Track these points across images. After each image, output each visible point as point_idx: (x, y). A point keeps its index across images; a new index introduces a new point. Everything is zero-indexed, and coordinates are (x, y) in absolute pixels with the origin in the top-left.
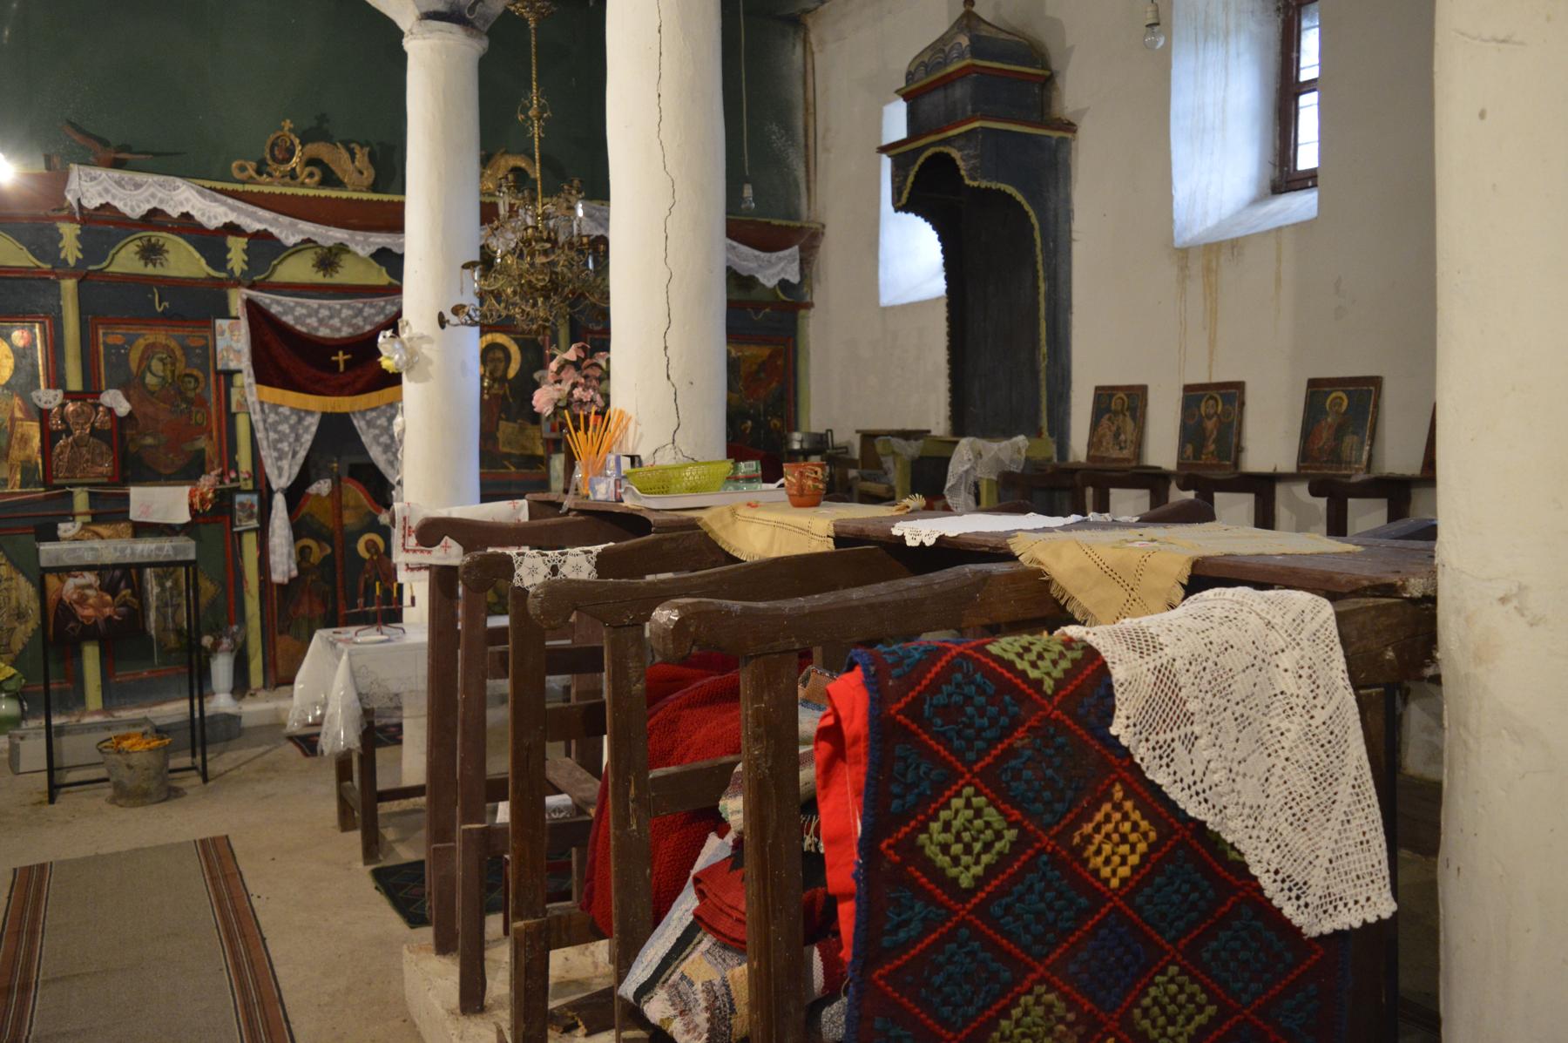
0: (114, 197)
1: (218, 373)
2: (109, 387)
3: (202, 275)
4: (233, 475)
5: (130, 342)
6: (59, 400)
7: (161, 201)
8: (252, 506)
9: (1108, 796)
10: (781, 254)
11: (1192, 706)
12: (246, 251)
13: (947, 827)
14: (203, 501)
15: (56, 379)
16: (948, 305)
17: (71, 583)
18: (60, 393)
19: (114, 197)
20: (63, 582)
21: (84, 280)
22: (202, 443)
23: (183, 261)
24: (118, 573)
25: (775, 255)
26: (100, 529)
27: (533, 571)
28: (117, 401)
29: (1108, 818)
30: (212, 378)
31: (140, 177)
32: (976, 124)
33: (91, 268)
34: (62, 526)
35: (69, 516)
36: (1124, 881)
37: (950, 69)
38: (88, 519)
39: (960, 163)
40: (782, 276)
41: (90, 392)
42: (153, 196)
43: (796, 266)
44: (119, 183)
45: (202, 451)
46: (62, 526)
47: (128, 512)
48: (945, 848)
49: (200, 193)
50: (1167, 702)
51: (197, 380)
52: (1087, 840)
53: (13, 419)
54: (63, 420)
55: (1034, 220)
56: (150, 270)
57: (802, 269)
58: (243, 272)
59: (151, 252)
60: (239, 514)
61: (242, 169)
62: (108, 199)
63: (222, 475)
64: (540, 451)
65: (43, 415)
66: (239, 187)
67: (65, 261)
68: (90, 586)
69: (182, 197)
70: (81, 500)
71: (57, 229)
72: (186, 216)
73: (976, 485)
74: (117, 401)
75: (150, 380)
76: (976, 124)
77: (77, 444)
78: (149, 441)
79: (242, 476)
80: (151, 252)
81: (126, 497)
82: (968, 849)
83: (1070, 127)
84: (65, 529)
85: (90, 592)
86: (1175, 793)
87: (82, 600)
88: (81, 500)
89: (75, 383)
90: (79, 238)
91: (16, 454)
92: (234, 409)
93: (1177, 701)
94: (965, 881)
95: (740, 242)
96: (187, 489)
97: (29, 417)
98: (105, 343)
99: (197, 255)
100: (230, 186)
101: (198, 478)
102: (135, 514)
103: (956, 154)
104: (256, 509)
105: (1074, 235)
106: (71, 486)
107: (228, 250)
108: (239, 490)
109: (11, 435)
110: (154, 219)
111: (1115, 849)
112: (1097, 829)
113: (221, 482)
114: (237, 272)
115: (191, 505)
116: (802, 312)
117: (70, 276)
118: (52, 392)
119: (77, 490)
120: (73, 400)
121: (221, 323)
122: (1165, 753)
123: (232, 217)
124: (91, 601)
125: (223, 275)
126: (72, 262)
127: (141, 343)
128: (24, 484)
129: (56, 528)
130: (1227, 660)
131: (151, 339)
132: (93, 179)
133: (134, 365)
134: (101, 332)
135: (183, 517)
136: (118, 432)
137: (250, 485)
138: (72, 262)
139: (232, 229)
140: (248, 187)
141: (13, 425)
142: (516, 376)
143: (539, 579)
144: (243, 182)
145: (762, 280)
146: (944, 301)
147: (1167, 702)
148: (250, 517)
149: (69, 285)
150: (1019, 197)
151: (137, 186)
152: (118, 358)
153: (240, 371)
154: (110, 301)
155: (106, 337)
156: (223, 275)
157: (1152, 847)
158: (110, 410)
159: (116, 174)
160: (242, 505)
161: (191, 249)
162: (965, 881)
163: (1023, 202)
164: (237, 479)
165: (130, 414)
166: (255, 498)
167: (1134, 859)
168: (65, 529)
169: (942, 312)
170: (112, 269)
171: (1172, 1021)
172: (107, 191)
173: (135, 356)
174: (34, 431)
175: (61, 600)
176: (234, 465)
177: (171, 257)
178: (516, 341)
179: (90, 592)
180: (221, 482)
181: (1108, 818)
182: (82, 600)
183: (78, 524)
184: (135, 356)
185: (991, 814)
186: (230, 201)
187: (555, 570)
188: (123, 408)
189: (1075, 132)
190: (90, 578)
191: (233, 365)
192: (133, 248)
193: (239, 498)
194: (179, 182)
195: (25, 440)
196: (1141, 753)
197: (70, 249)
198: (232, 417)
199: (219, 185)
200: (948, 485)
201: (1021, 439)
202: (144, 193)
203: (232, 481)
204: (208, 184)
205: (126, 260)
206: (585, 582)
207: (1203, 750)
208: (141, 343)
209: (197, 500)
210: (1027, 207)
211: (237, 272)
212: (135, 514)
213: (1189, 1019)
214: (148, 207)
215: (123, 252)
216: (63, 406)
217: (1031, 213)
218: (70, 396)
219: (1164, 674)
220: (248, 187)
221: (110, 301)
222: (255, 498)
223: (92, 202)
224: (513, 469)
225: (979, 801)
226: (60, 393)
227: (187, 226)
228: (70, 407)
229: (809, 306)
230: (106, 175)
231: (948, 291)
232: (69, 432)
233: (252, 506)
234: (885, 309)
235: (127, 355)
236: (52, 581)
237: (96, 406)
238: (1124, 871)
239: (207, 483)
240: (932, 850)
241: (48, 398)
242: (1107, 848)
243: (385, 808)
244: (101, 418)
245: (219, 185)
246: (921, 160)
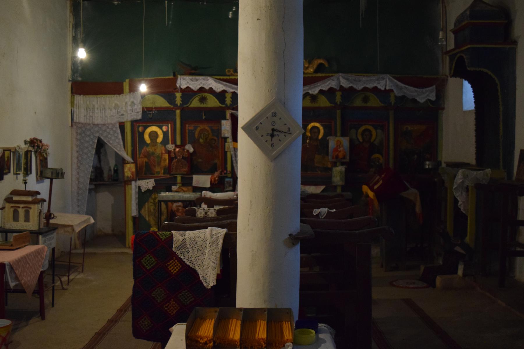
0: (190, 84)
1: (222, 138)
2: (189, 143)
3: (218, 106)
4: (225, 172)
5: (196, 128)
6: (174, 148)
7: (203, 84)
8: (230, 182)
9: (173, 259)
10: (427, 89)
11: (188, 246)
12: (231, 98)
13: (146, 260)
14: (215, 180)
15: (174, 142)
16: (475, 113)
17: (175, 205)
18: (174, 145)
19: (190, 84)
20: (173, 204)
21: (182, 110)
22: (216, 161)
23: (212, 102)
24: (188, 203)
25: (425, 90)
26: (184, 188)
27: (201, 213)
28: (190, 148)
29: (172, 262)
30: (220, 140)
31: (198, 77)
32: (469, 46)
33: (185, 106)
34: (173, 187)
35: (175, 184)
36: (175, 273)
37: (463, 24)
38: (181, 185)
39: (466, 60)
40: (428, 98)
41: (183, 144)
42: (201, 83)
43: (434, 94)
44: (192, 80)
45: (216, 164)
46: (173, 187)
47: (192, 183)
48: (145, 263)
49: (215, 81)
50: (183, 245)
51: (215, 140)
52: (169, 265)
53: (162, 153)
54: (175, 154)
55: (497, 82)
56: (202, 105)
57: (437, 96)
58: (230, 104)
59: (203, 100)
60: (227, 185)
61: (229, 71)
62: (188, 85)
63: (222, 171)
64: (330, 166)
65: (169, 152)
66: (228, 77)
67: (177, 104)
68: (180, 206)
69: (210, 83)
70: (179, 179)
71: (175, 95)
72: (211, 89)
73: (467, 188)
74: (190, 148)
75: (201, 140)
76: (469, 46)
77: (178, 161)
78: (200, 160)
79: (228, 172)
80: (203, 100)
81: (192, 178)
82: (149, 263)
83: (515, 43)
84: (174, 188)
85: (180, 208)
86: (184, 260)
87: (178, 210)
88: (179, 179)
89: (178, 143)
90: (181, 97)
91: (163, 164)
92: (226, 150)
93: (186, 245)
94: (148, 268)
95: (409, 85)
96: (210, 176)
97: (166, 153)
98: (188, 130)
99: (216, 100)
100: (225, 77)
101: (214, 173)
102: (194, 184)
103: (465, 57)
104: (232, 183)
105: (517, 87)
106: (177, 174)
107: (226, 98)
108: (227, 177)
109: (161, 158)
110: (202, 90)
111: (174, 268)
112: (171, 264)
113: (221, 174)
114: (228, 104)
115: (211, 182)
116: (440, 111)
117: (178, 109)
118: (172, 145)
119: (178, 176)
120: (178, 148)
121: (223, 122)
122: (183, 253)
123: (224, 88)
124: (180, 211)
125: (224, 106)
126: (179, 104)
127: (199, 129)
128: (164, 174)
129: (171, 188)
130: (197, 239)
131: (202, 127)
132: (184, 79)
133: (196, 136)
134: (187, 126)
135: (208, 185)
136: (190, 158)
137: (230, 175)
138: (179, 104)
139: (224, 92)
140: (231, 77)
141: (162, 155)
142: (322, 138)
143: (202, 216)
144: (229, 76)
145: (418, 100)
146: (474, 111)
147: (183, 245)
148: (230, 186)
149: (178, 112)
150: (490, 73)
151: (197, 80)
152: (192, 133)
153: (228, 137)
154: (190, 116)
155: (189, 127)
156: (224, 106)
157: (180, 268)
158: (188, 151)
159: (191, 77)
160: (227, 181)
161: (214, 98)
162: (148, 268)
163: (492, 75)
164: (227, 173)
165: (194, 152)
166: (231, 180)
167: (177, 270)
168: (174, 188)
169: (473, 116)
170: (191, 106)
171: (186, 299)
172: (188, 82)
173: (197, 133)
174: (166, 156)
175: (172, 210)
176: (226, 169)
177: (209, 101)
178: (322, 125)
179: (180, 208)
180: (221, 174)
181: (172, 262)
182: (178, 210)
183: (178, 187)
184: (197, 133)
185: (153, 259)
186: (224, 83)
187: (206, 213)
188: (191, 150)
189: (517, 45)
190: (180, 204)
191: (226, 135)
192: (197, 99)
193: (227, 180)
194: (209, 78)
195: (165, 160)
196: (178, 252)
197: (179, 101)
198: (226, 153)
199: (222, 77)
200: (454, 187)
201: (488, 171)
202: (199, 82)
203: (225, 174)
204: (218, 77)
205: (195, 103)
206: (213, 217)
207: (191, 254)
208: (199, 129)
209: (213, 180)
210: (494, 76)
211: (228, 104)
212: (194, 184)
213: (190, 300)
214: (199, 87)
215: (194, 100)
216: (175, 149)
217: (496, 79)
218: (177, 146)
219: (184, 240)
220: (231, 77)
221: (190, 116)
222: (231, 180)
223: (184, 87)
224: (319, 172)
225: (151, 256)
226: (174, 145)
227: (211, 91)
228: (177, 150)
229: (443, 109)
230: (188, 78)
231: (475, 108)
232: (176, 157)
233: (230, 182)
234: (465, 112)
235: (194, 133)
236: (170, 204)
237: (184, 149)
238: (175, 271)
239: (217, 174)
240: (143, 263)
241: (170, 147)
242: (172, 267)
243: (5, 234)
244: (186, 154)
245: (222, 77)
246: (456, 58)
